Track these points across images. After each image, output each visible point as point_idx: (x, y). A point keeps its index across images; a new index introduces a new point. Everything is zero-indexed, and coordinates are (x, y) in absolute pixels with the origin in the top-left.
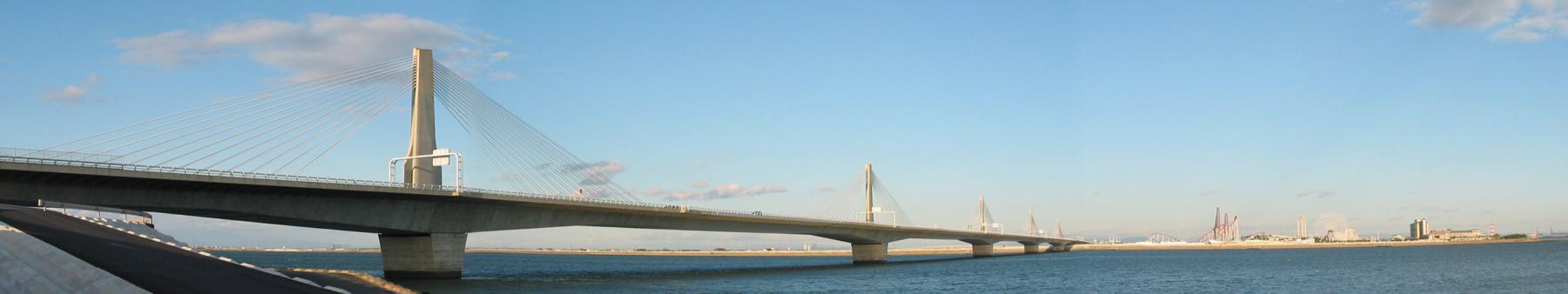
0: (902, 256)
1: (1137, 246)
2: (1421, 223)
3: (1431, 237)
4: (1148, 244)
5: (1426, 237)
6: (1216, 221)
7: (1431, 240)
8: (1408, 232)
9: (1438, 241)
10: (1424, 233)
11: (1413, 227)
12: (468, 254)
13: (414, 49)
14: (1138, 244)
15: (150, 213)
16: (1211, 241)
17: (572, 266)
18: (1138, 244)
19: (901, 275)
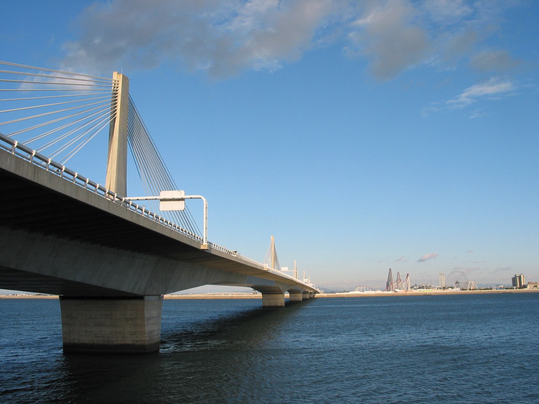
0: (362, 295)
1: (351, 295)
2: (520, 277)
3: (528, 286)
4: (357, 293)
5: (525, 287)
6: (389, 273)
7: (529, 289)
8: (510, 283)
9: (535, 289)
10: (523, 284)
11: (514, 280)
12: (116, 71)
13: (272, 236)
14: (351, 293)
15: (181, 191)
16: (397, 290)
17: (370, 333)
18: (351, 293)
19: (70, 70)
